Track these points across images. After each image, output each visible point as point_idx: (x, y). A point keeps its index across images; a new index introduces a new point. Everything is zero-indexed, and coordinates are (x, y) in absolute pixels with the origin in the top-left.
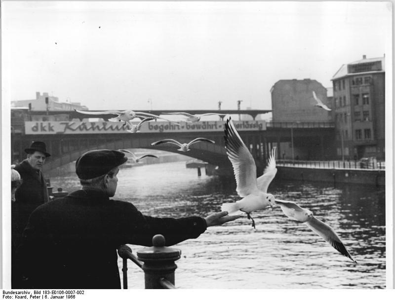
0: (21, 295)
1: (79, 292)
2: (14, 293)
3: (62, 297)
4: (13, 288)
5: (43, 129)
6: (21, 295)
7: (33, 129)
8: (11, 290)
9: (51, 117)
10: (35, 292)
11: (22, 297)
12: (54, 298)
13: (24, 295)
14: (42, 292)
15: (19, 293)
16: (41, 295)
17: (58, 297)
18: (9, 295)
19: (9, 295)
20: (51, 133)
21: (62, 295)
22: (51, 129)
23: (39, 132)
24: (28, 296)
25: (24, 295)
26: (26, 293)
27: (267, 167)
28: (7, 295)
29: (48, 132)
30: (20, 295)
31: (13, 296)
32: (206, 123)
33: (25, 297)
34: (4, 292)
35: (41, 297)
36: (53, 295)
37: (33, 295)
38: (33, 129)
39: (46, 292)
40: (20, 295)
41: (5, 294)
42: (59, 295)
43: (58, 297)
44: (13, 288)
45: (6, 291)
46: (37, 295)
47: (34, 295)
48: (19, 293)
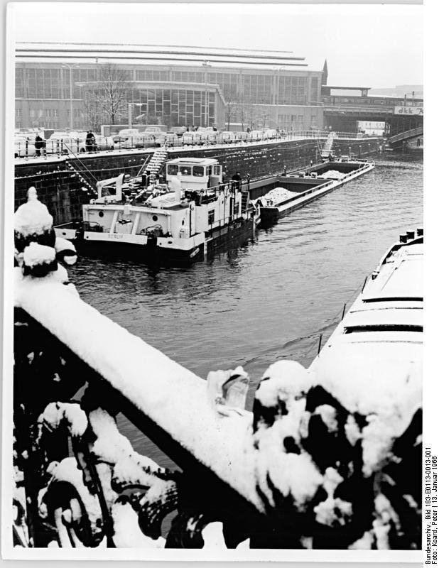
0: (432, 538)
1: (428, 454)
2: (428, 548)
3: (435, 475)
4: (419, 548)
5: (405, 111)
6: (432, 538)
7: (399, 111)
8: (423, 552)
9: (410, 103)
10: (428, 518)
11: (435, 537)
12: (435, 486)
13: (432, 533)
14: (428, 508)
15: (429, 540)
16: (432, 509)
17: (435, 482)
18: (432, 554)
19: (432, 554)
20: (410, 114)
21: (432, 513)
22: (410, 112)
23: (403, 114)
24: (433, 528)
25: (432, 533)
26: (429, 530)
27: (200, 461)
28: (432, 558)
29: (408, 114)
30: (432, 539)
31: (432, 548)
32: (412, 132)
33: (435, 532)
34: (428, 562)
35: (435, 471)
36: (432, 488)
37: (432, 520)
38: (399, 111)
39: (428, 502)
40: (432, 539)
41: (431, 561)
42: (432, 480)
43: (435, 482)
44: (419, 548)
45: (426, 559)
46: (432, 515)
47: (432, 519)
48: (429, 540)
